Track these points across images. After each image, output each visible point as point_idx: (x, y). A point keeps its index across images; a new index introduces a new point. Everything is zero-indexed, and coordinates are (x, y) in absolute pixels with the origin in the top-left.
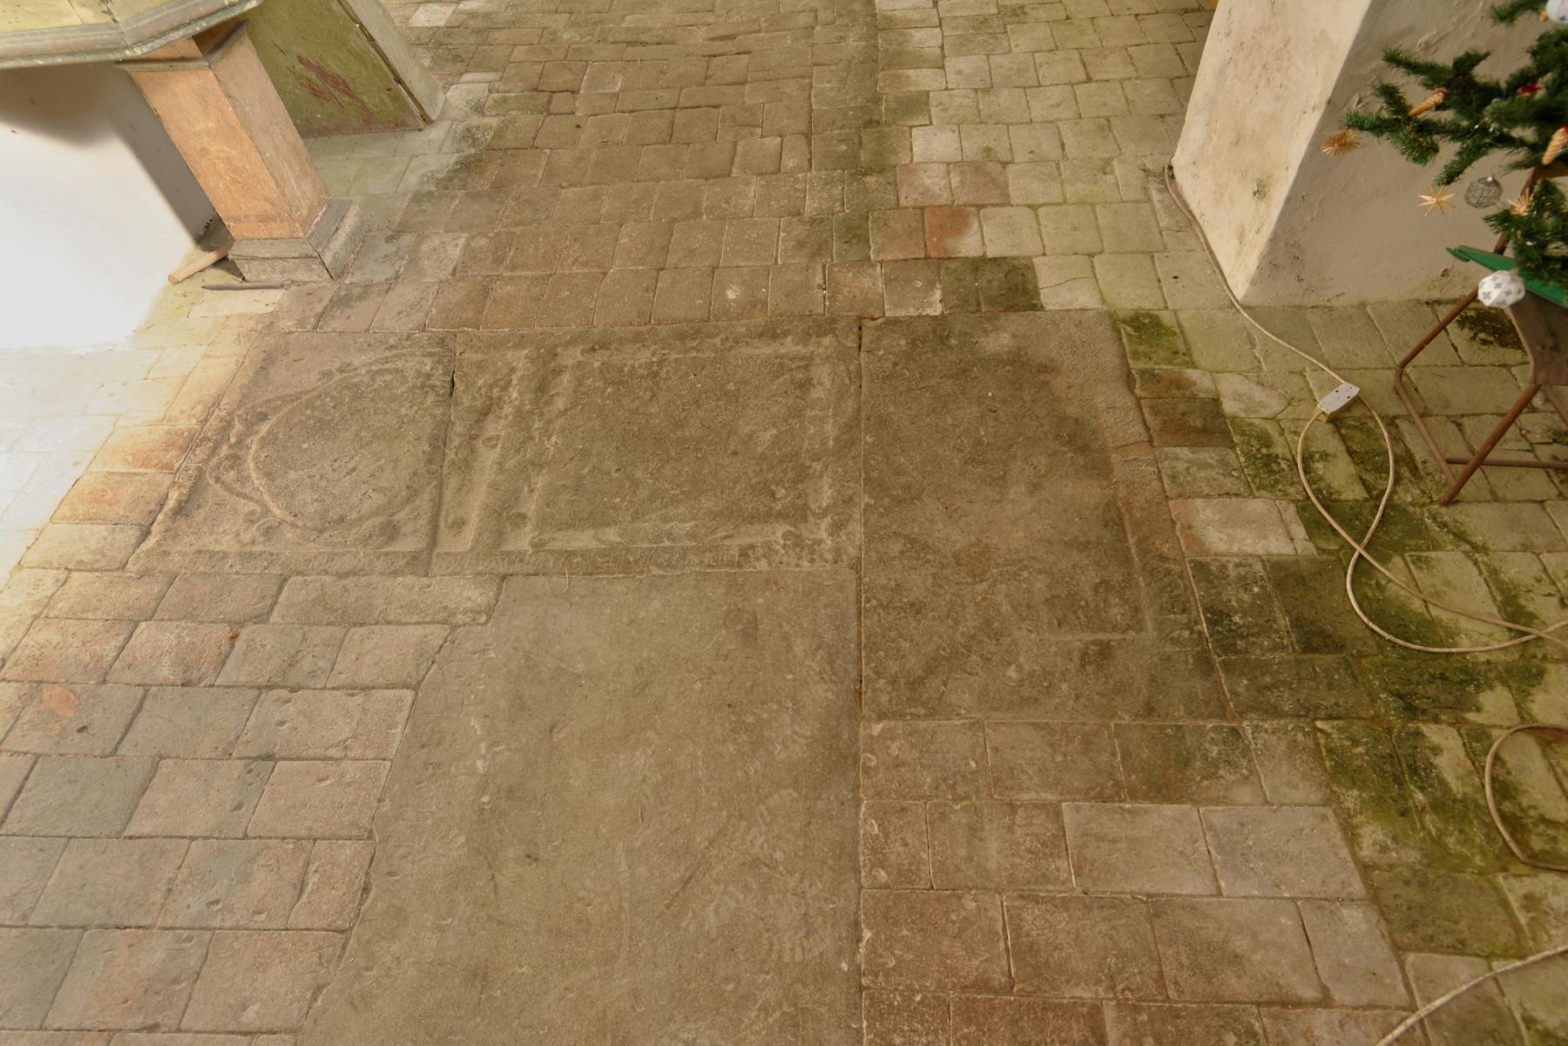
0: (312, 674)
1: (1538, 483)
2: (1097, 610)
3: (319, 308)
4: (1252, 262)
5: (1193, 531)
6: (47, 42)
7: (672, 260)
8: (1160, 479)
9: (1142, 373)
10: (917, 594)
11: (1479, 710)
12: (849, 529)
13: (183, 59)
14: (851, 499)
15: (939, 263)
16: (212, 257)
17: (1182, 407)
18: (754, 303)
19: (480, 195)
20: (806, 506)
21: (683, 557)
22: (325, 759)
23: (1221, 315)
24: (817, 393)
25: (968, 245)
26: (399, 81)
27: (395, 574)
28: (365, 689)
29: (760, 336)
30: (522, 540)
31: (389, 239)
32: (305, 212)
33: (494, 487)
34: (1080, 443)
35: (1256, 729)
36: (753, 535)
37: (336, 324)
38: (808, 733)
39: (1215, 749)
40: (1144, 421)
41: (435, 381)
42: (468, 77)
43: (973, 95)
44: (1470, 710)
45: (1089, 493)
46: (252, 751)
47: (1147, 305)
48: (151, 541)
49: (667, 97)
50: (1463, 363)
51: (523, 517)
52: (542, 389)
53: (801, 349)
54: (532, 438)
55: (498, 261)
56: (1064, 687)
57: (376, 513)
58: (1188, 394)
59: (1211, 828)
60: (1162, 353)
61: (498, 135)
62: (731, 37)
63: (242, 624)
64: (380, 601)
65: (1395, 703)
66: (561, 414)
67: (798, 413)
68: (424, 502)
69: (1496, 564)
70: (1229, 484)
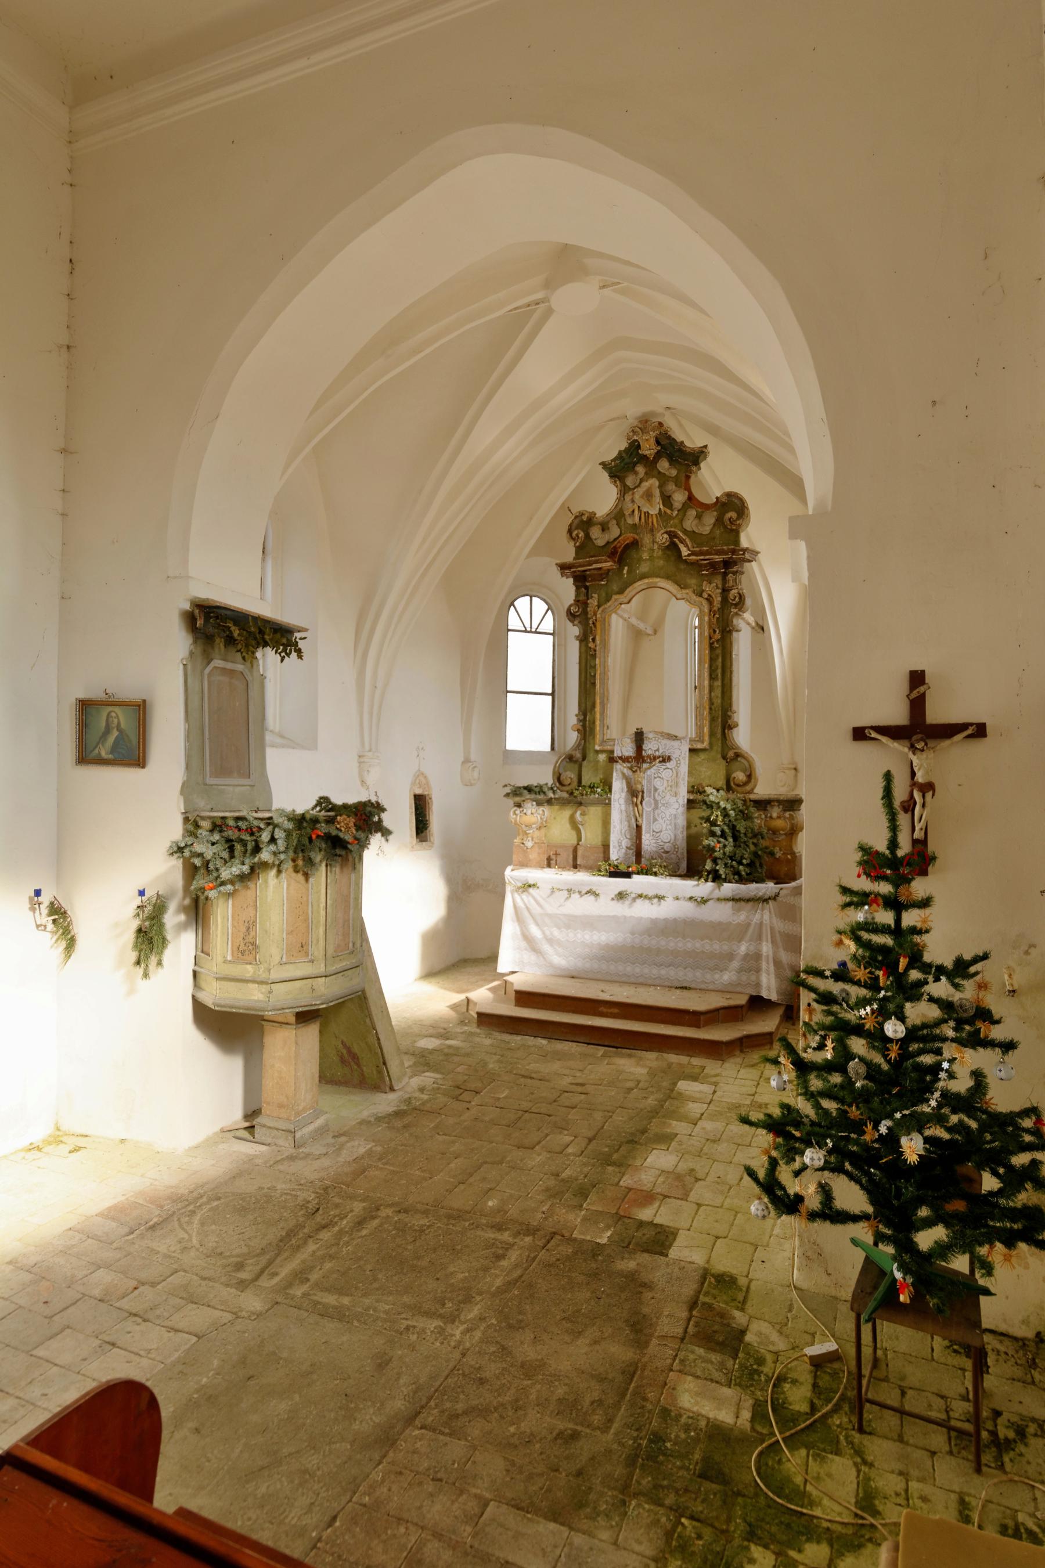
0: (158, 1317)
1: (938, 1439)
2: (586, 1413)
3: (279, 1158)
5: (674, 1392)
6: (241, 1004)
7: (471, 1180)
8: (674, 1360)
9: (704, 1304)
10: (487, 1374)
11: (800, 1551)
12: (474, 1333)
13: (287, 1024)
14: (485, 1318)
16: (247, 1124)
17: (716, 1328)
18: (500, 1210)
19: (394, 1128)
20: (458, 1316)
21: (374, 1321)
22: (137, 1354)
23: (780, 1289)
24: (504, 1263)
25: (645, 1214)
26: (384, 1063)
27: (227, 1285)
28: (177, 1331)
29: (492, 1227)
30: (298, 1291)
31: (334, 1137)
32: (301, 1108)
33: (303, 1262)
34: (639, 1329)
35: (639, 1505)
36: (420, 1322)
37: (281, 1167)
38: (377, 1421)
39: (605, 1506)
40: (687, 1327)
41: (310, 1206)
42: (427, 1074)
43: (704, 1141)
44: (794, 1549)
45: (620, 1352)
46: (107, 1339)
47: (734, 1271)
48: (132, 1236)
49: (525, 1105)
50: (933, 1359)
51: (308, 1280)
52: (360, 1223)
53: (511, 1240)
54: (338, 1245)
55: (380, 1159)
56: (538, 1446)
57: (238, 1256)
58: (725, 1322)
59: (571, 1544)
60: (725, 1298)
61: (423, 1104)
62: (582, 1085)
63: (143, 1284)
64: (212, 1296)
65: (743, 1526)
66: (362, 1237)
67: (486, 1269)
68: (264, 1260)
69: (872, 1476)
70: (717, 1375)
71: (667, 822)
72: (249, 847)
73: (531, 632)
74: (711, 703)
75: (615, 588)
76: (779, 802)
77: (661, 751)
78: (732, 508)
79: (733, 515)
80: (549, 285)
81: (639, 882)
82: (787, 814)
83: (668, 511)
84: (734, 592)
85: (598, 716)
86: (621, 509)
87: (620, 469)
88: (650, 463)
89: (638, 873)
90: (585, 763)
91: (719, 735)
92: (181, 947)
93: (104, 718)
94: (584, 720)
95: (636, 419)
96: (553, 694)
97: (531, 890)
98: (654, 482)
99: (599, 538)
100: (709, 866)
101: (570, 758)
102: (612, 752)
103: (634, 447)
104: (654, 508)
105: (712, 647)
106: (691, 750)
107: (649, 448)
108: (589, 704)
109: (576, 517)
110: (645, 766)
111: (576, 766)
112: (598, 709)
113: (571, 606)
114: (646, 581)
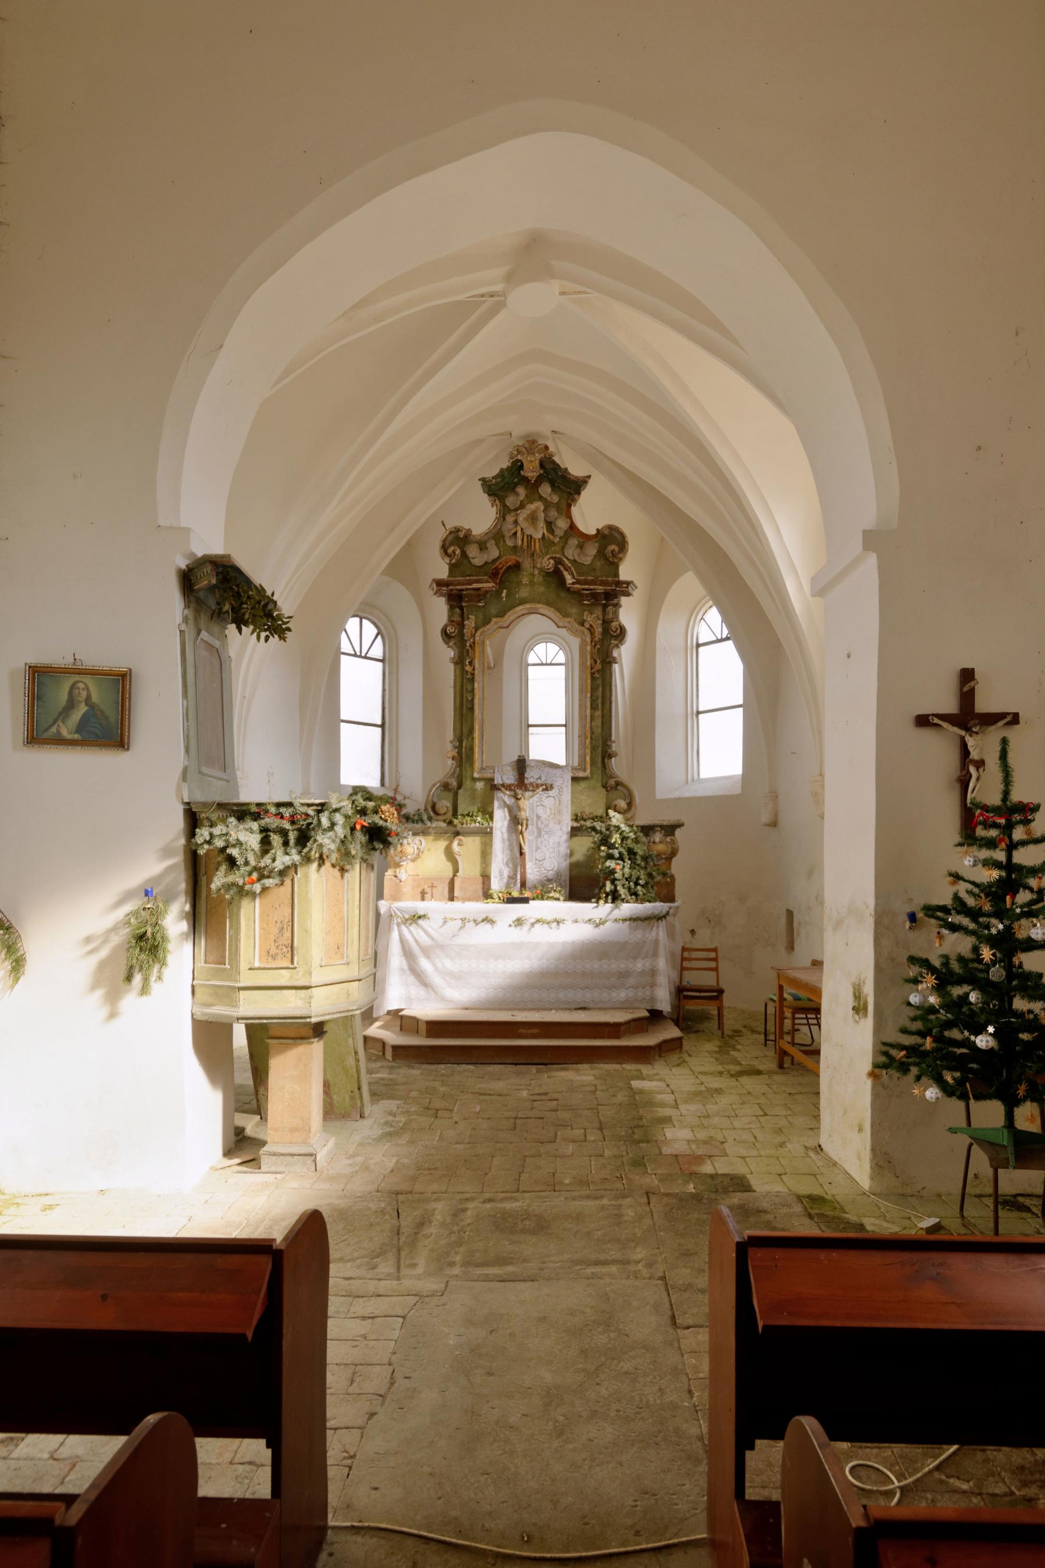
4: (867, 1166)
15: (692, 1175)
25: (707, 1168)
62: (546, 1094)
71: (551, 849)
72: (292, 836)
73: (360, 656)
74: (592, 733)
75: (493, 611)
76: (662, 827)
77: (543, 779)
78: (611, 542)
79: (613, 547)
80: (511, 278)
81: (537, 908)
82: (668, 839)
83: (551, 537)
84: (614, 624)
85: (477, 741)
86: (500, 529)
87: (499, 488)
88: (533, 487)
89: (533, 899)
90: (461, 791)
91: (599, 765)
92: (182, 957)
93: (67, 689)
94: (460, 747)
95: (521, 437)
96: (382, 726)
97: (420, 922)
98: (539, 505)
99: (477, 558)
100: (609, 887)
101: (446, 786)
102: (493, 780)
103: (517, 467)
104: (539, 532)
105: (593, 678)
106: (574, 779)
107: (531, 470)
108: (465, 730)
109: (451, 532)
110: (527, 794)
111: (451, 795)
112: (477, 734)
113: (446, 626)
114: (528, 606)
